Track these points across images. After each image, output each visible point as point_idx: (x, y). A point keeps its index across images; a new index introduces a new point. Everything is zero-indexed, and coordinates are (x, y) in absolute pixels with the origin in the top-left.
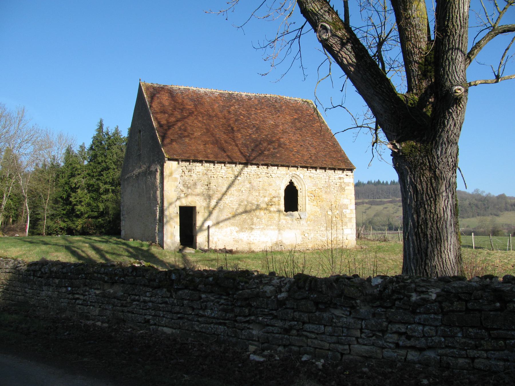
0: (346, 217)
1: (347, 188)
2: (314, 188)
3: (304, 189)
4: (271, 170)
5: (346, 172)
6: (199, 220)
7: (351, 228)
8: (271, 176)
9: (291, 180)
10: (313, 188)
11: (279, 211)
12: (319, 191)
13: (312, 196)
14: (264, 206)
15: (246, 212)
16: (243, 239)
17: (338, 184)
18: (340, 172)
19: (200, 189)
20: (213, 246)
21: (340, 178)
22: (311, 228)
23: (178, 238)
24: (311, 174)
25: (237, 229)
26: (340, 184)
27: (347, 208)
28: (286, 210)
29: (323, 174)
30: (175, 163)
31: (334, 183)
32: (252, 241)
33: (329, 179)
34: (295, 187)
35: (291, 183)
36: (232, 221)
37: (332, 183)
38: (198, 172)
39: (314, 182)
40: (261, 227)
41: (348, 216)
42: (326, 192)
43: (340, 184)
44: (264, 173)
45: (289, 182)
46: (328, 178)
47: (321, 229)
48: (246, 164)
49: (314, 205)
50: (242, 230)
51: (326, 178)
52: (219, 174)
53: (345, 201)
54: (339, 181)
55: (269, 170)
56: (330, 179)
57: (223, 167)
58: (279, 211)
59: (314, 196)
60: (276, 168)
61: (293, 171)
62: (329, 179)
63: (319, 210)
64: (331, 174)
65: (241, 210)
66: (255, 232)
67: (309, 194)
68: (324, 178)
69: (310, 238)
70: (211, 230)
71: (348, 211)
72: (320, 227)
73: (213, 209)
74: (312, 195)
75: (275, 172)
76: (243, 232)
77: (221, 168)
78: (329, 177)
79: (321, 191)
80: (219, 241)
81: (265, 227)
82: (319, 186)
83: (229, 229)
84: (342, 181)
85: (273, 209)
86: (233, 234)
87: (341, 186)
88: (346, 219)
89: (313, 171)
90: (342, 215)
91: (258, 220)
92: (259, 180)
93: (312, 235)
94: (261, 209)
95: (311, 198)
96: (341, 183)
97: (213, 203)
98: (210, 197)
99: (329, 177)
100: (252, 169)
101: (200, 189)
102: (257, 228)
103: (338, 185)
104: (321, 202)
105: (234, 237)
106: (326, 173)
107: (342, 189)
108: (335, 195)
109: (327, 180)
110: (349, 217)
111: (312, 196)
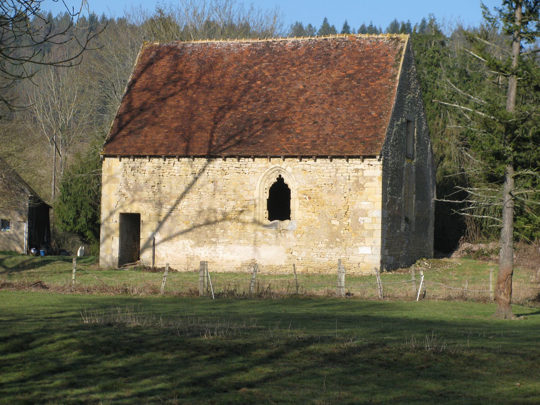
0: (363, 228)
1: (368, 184)
2: (309, 187)
3: (261, 191)
4: (243, 163)
5: (367, 161)
6: (145, 234)
7: (372, 246)
8: (242, 172)
9: (280, 176)
10: (308, 186)
11: (256, 222)
12: (318, 191)
13: (306, 198)
14: (233, 215)
15: (208, 223)
16: (199, 256)
17: (353, 179)
18: (358, 161)
19: (146, 193)
20: (158, 265)
21: (357, 170)
22: (303, 244)
23: (116, 254)
24: (306, 167)
25: (192, 242)
26: (355, 178)
27: (367, 216)
28: (271, 217)
29: (326, 165)
30: (115, 160)
31: (345, 179)
32: (213, 259)
33: (336, 172)
34: (287, 185)
35: (280, 180)
36: (190, 234)
37: (342, 178)
38: (143, 170)
39: (311, 178)
40: (226, 240)
41: (366, 228)
42: (329, 192)
43: (355, 178)
44: (233, 168)
45: (277, 179)
46: (335, 170)
47: (319, 246)
48: (211, 156)
49: (308, 211)
50: (199, 244)
51: (331, 171)
52: (170, 171)
53: (364, 205)
54: (356, 174)
55: (240, 163)
56: (339, 171)
57: (177, 162)
58: (256, 222)
59: (310, 198)
60: (250, 159)
61: (276, 163)
62: (336, 172)
63: (316, 218)
64: (340, 165)
65: (201, 221)
66: (220, 247)
67: (301, 195)
68: (328, 171)
69: (300, 258)
70: (157, 248)
71: (367, 220)
72: (317, 242)
73: (166, 218)
74: (305, 196)
75: (249, 165)
76: (199, 246)
77: (174, 164)
78: (337, 170)
79: (321, 191)
80: (167, 257)
81: (232, 240)
82: (318, 183)
83: (181, 242)
84: (360, 173)
85: (248, 218)
86: (186, 249)
87: (357, 182)
88: (363, 231)
89: (311, 162)
90: (357, 227)
91: (222, 231)
92: (225, 177)
93: (304, 254)
94: (230, 219)
95: (304, 200)
96: (357, 177)
97: (165, 211)
98: (160, 204)
99: (337, 170)
100: (219, 162)
101: (146, 193)
102: (220, 241)
103: (352, 181)
104: (320, 207)
105: (187, 253)
106: (332, 163)
107: (359, 186)
108: (345, 195)
109: (333, 174)
110: (370, 228)
111: (306, 198)
